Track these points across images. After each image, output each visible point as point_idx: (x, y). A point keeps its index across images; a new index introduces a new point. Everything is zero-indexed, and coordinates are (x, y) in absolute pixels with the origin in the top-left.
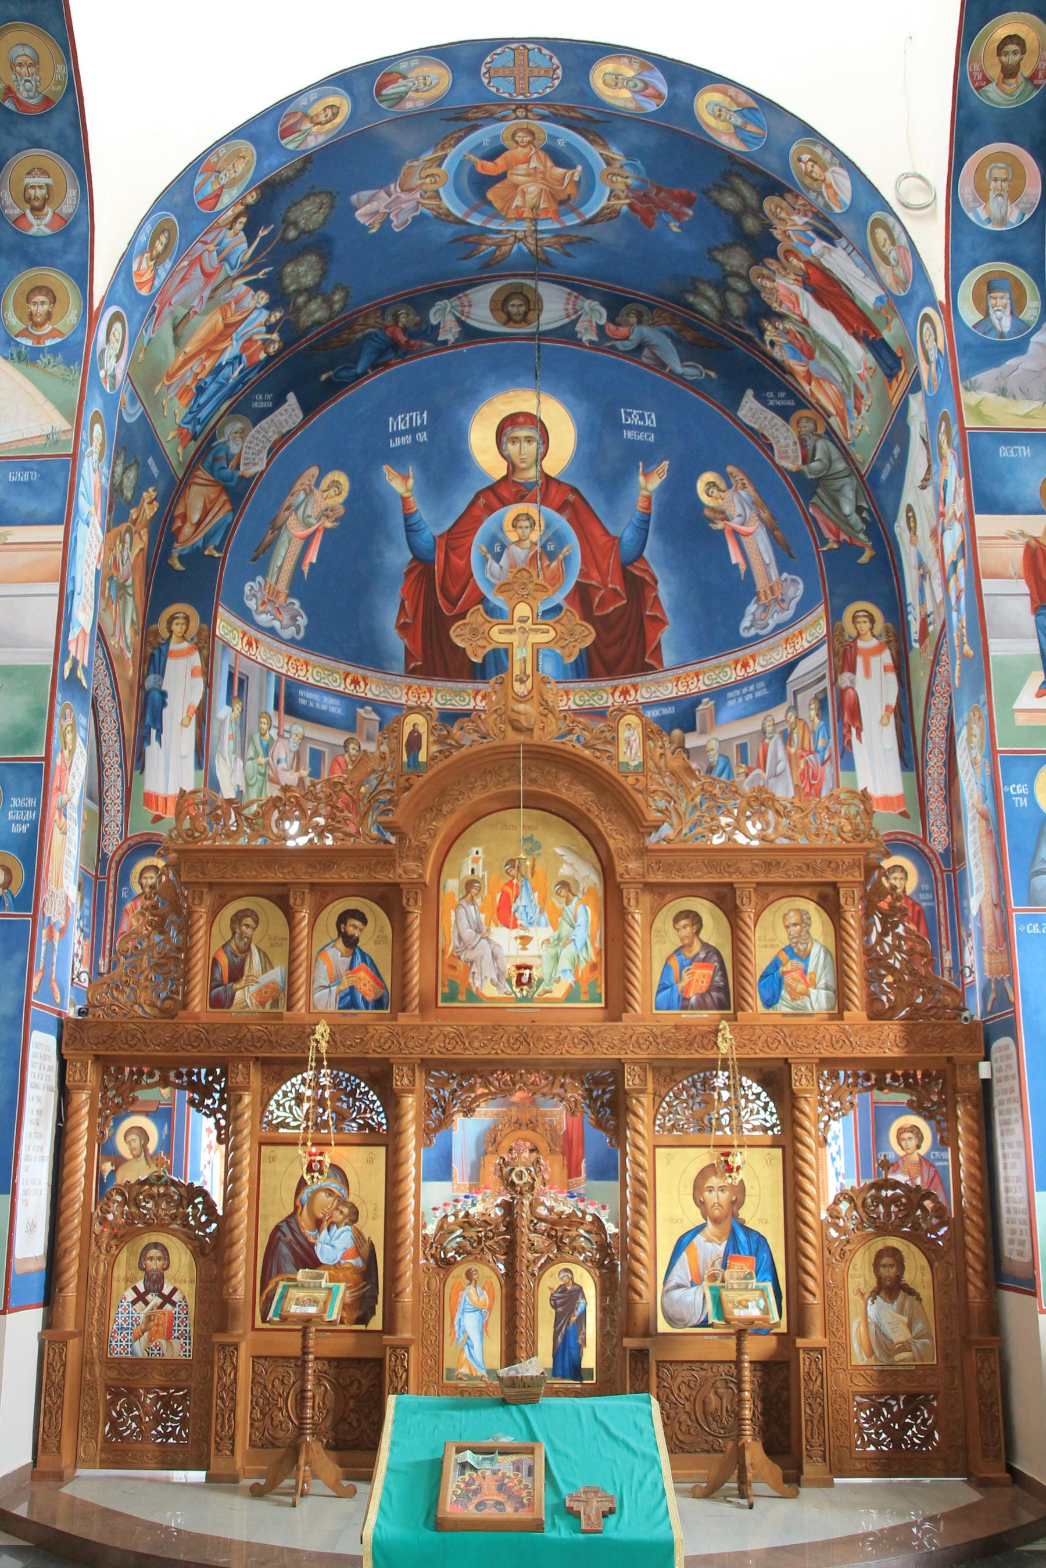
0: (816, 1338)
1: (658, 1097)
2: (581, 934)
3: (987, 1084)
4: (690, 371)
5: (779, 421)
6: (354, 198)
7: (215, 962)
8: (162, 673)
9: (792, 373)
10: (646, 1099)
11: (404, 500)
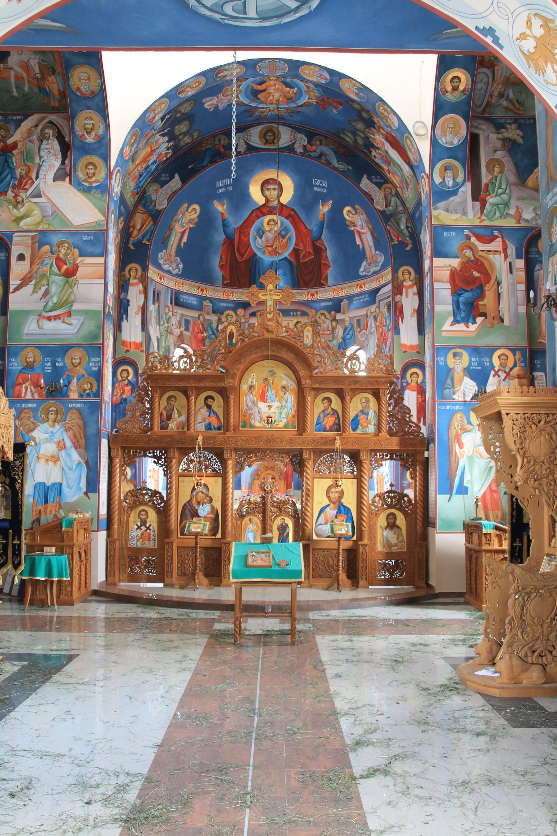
0: (366, 541)
1: (315, 461)
2: (289, 405)
3: (427, 459)
4: (341, 166)
5: (377, 188)
6: (204, 100)
7: (162, 414)
8: (127, 292)
9: (382, 168)
10: (311, 462)
11: (222, 214)
